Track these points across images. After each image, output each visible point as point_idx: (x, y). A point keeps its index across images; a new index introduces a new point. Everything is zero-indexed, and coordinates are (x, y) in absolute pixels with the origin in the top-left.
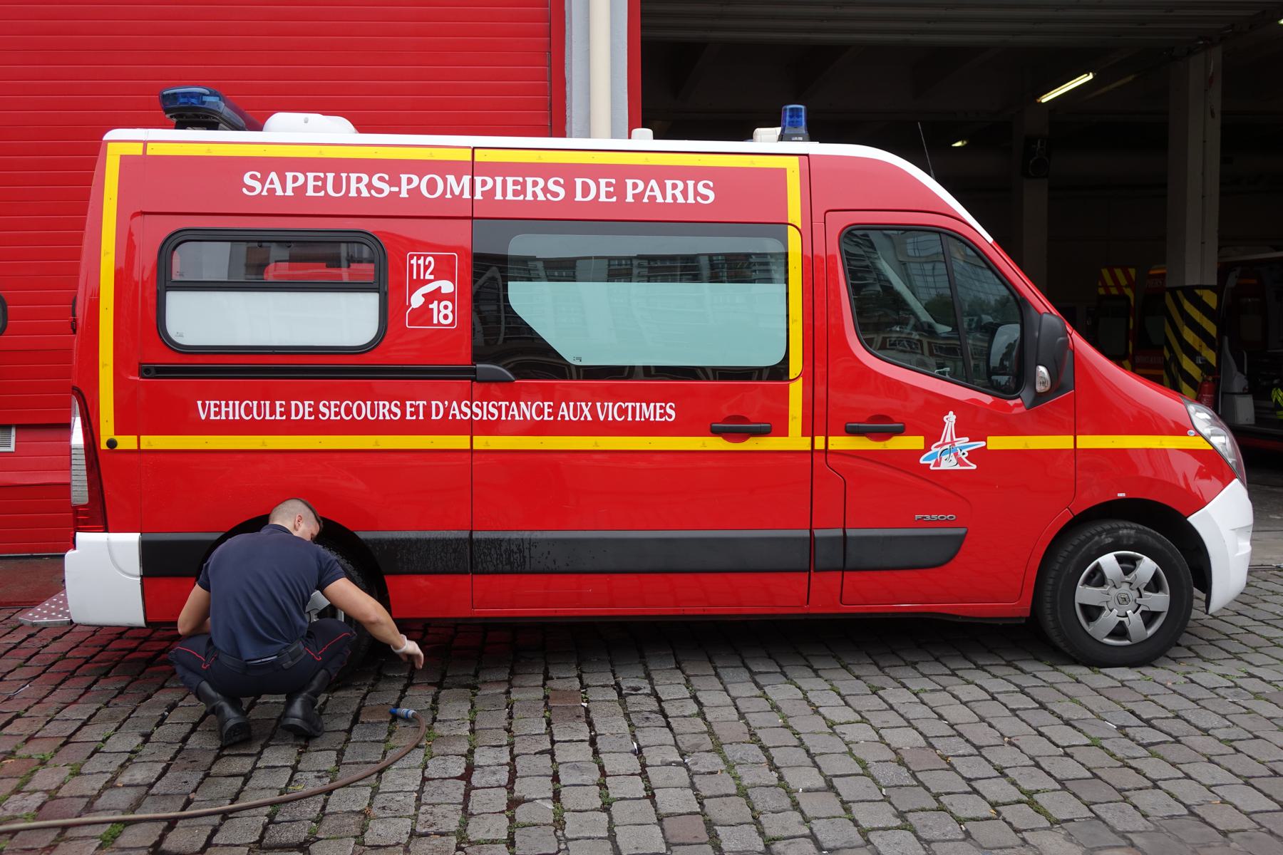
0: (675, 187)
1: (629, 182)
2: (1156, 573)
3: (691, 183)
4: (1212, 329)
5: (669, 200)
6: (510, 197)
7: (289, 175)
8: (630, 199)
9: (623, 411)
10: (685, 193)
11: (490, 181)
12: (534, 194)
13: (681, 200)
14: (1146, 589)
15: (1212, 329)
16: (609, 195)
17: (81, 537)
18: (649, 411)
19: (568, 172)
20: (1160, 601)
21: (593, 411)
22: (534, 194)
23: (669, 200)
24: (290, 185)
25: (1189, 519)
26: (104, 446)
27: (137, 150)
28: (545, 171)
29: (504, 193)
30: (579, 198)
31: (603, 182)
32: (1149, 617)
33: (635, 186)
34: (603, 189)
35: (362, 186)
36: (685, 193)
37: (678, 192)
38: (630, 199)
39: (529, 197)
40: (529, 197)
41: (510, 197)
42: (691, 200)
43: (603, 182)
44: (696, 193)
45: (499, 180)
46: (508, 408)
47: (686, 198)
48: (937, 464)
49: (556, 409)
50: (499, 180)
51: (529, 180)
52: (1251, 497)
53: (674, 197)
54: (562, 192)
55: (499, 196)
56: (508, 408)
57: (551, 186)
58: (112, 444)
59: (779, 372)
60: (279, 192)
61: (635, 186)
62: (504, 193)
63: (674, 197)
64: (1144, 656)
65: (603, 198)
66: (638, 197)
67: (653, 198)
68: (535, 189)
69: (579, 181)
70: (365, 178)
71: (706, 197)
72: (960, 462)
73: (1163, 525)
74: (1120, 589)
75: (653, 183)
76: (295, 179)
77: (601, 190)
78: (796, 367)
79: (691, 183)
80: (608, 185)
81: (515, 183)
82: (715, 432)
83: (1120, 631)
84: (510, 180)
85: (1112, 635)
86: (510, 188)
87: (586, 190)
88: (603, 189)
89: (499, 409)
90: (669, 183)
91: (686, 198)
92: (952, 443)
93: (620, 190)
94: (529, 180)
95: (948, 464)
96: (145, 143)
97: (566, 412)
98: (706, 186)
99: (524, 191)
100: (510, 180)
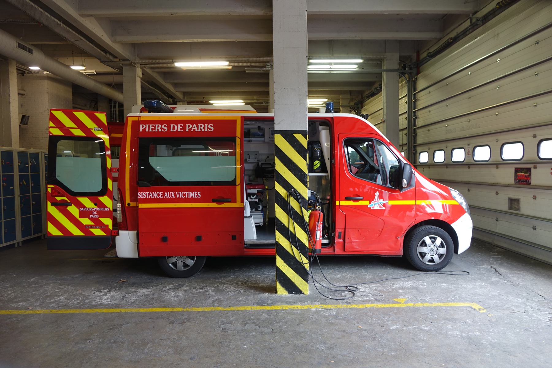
0: (201, 126)
1: (187, 125)
2: (442, 242)
3: (206, 125)
4: (280, 167)
5: (199, 130)
6: (150, 130)
7: (199, 125)
8: (187, 130)
9: (184, 195)
10: (204, 128)
11: (145, 126)
12: (158, 130)
13: (203, 130)
14: (439, 247)
15: (280, 167)
16: (181, 129)
17: (120, 232)
18: (193, 195)
19: (168, 122)
20: (443, 251)
21: (175, 195)
22: (158, 130)
23: (199, 130)
24: (199, 128)
25: (452, 225)
26: (127, 205)
27: (137, 119)
28: (161, 122)
29: (149, 130)
30: (172, 130)
31: (179, 125)
32: (441, 256)
33: (189, 126)
34: (179, 127)
35: (159, 128)
36: (204, 128)
37: (202, 128)
38: (187, 130)
39: (156, 130)
40: (156, 130)
41: (150, 130)
42: (206, 130)
43: (179, 125)
44: (208, 128)
45: (147, 125)
46: (149, 194)
47: (205, 130)
48: (373, 207)
49: (164, 194)
50: (147, 125)
51: (157, 125)
52: (472, 219)
53: (201, 129)
54: (166, 129)
55: (147, 130)
56: (149, 194)
57: (163, 127)
58: (129, 204)
59: (233, 183)
60: (196, 130)
61: (189, 126)
62: (149, 130)
63: (201, 129)
64: (436, 269)
65: (179, 130)
66: (190, 130)
67: (194, 130)
68: (158, 128)
69: (172, 125)
70: (160, 126)
71: (211, 129)
72: (380, 207)
73: (443, 227)
74: (432, 248)
75: (195, 125)
76: (143, 127)
77: (178, 128)
78: (238, 182)
79: (206, 125)
80: (181, 126)
81: (152, 126)
82: (213, 201)
83: (432, 260)
84: (151, 125)
85: (429, 261)
86: (151, 128)
87: (174, 129)
88: (179, 127)
89: (146, 194)
90: (199, 125)
91: (205, 130)
92: (378, 201)
93: (184, 128)
94: (157, 125)
95: (377, 207)
96: (139, 117)
97: (167, 195)
98: (211, 126)
99: (155, 129)
100: (151, 125)
